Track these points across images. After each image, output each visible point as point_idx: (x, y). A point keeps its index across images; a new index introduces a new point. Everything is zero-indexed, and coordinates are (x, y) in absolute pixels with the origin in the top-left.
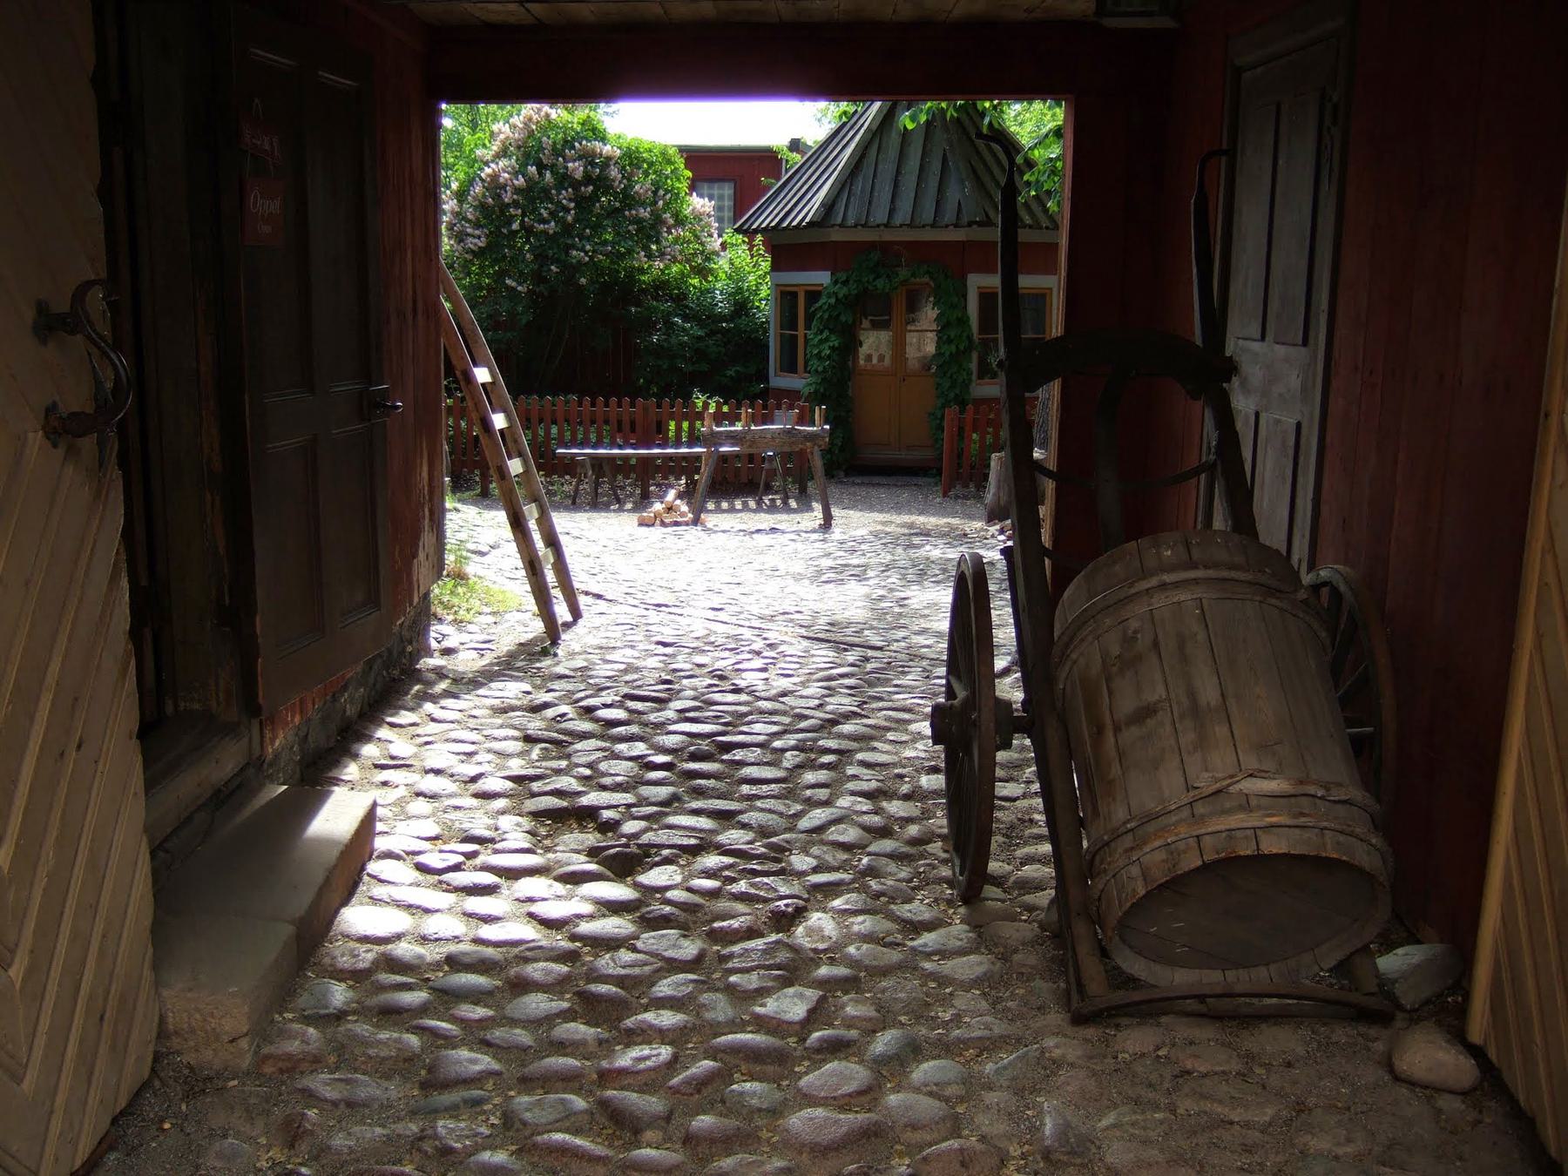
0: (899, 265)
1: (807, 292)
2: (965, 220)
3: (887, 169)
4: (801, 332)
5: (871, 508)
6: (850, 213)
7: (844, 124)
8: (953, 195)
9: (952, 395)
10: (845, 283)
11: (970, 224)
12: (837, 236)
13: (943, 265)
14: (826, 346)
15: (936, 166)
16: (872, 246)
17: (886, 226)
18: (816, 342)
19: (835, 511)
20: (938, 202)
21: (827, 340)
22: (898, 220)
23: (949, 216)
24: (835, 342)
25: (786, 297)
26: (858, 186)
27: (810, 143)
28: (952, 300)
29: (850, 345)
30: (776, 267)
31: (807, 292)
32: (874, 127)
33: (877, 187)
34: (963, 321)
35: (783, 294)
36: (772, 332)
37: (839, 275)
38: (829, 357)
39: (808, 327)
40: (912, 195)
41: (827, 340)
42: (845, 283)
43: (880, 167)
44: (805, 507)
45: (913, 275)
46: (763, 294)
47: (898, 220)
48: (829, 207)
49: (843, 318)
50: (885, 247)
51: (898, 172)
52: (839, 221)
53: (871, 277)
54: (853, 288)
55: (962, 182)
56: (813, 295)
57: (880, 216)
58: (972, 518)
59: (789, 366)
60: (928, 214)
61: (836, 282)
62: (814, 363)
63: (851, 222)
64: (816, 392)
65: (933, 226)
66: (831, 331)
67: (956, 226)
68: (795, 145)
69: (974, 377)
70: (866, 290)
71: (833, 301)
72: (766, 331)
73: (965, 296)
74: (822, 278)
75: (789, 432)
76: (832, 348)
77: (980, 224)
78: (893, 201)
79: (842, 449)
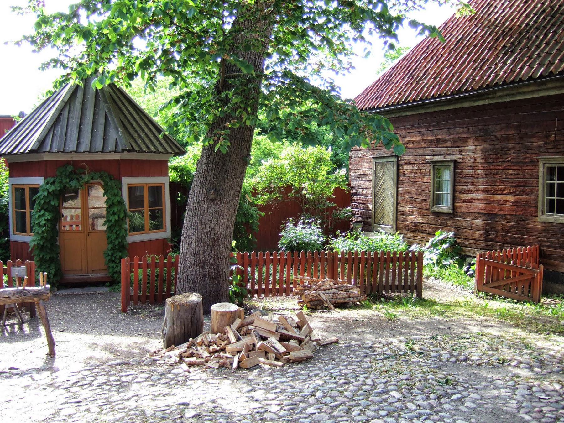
0: (84, 173)
1: (30, 188)
2: (120, 148)
3: (74, 121)
4: (27, 210)
5: (80, 330)
6: (54, 145)
7: (50, 98)
8: (113, 135)
9: (117, 243)
10: (53, 183)
11: (123, 151)
12: (47, 157)
13: (108, 174)
14: (43, 219)
15: (102, 120)
16: (68, 163)
17: (76, 152)
18: (37, 216)
19: (57, 336)
20: (104, 139)
21: (43, 215)
22: (82, 149)
23: (111, 146)
24: (48, 216)
25: (19, 191)
26: (59, 130)
27: (55, 364)
28: (112, 190)
29: (57, 217)
30: (11, 175)
31: (30, 188)
32: (66, 99)
33: (69, 131)
34: (121, 203)
35: (16, 189)
36: (10, 210)
37: (49, 179)
38: (45, 225)
39: (32, 207)
40: (90, 135)
41: (43, 215)
42: (53, 183)
43: (70, 121)
44: (35, 334)
45: (92, 178)
46: (5, 189)
47: (82, 149)
48: (42, 142)
49: (52, 203)
50: (75, 163)
51: (81, 123)
52: (48, 149)
53: (68, 180)
54: (57, 187)
55: (117, 129)
56: (34, 190)
57: (72, 146)
58: (149, 335)
59: (22, 229)
60: (99, 145)
61: (47, 183)
62: (36, 228)
63: (55, 150)
64: (38, 244)
65: (102, 152)
66: (46, 210)
67: (115, 152)
68: (22, 115)
69: (128, 232)
70: (65, 187)
71: (46, 194)
72: (7, 208)
73: (121, 189)
74: (39, 181)
75: (21, 292)
76: (47, 220)
77: (129, 151)
78: (79, 138)
79: (55, 275)
